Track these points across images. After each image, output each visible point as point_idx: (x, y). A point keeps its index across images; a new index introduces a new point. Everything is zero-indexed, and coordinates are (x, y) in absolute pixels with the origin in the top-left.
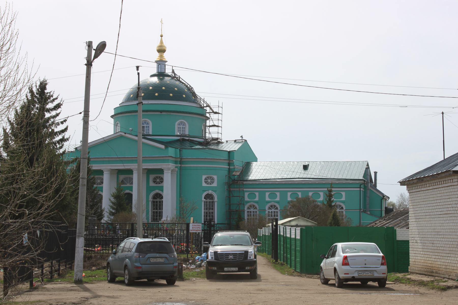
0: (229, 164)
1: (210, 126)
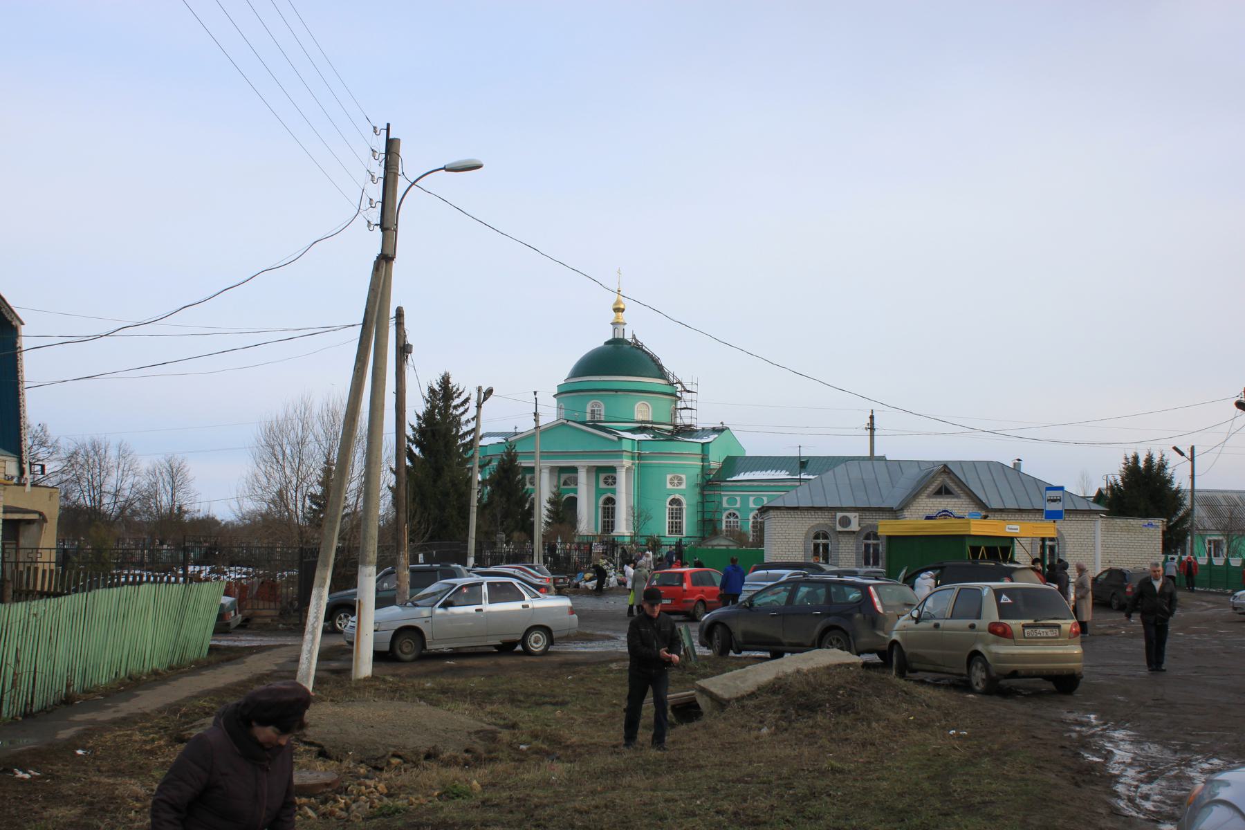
0: (703, 460)
1: (681, 409)
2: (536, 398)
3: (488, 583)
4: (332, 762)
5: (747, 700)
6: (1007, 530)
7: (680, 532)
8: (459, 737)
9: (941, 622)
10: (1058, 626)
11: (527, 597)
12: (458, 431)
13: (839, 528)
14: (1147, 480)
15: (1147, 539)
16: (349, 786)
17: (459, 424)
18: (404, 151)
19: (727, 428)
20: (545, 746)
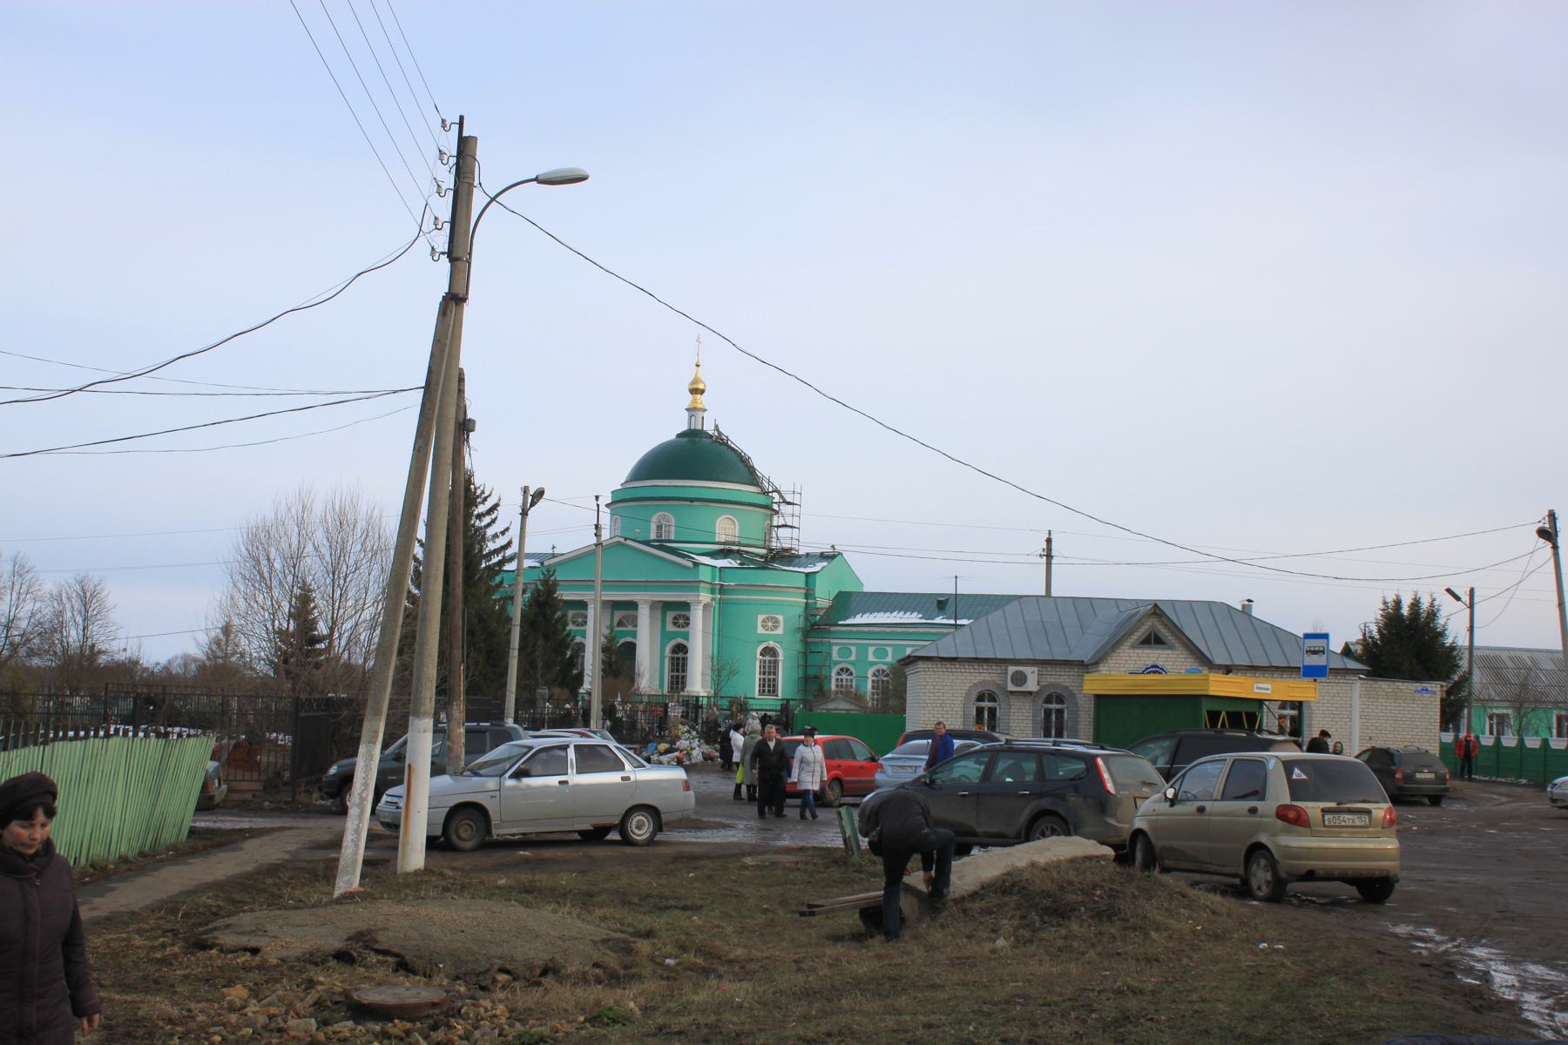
0: (807, 596)
1: (778, 527)
2: (598, 505)
3: (575, 746)
4: (417, 978)
5: (968, 901)
6: (1256, 690)
7: (774, 691)
8: (582, 947)
9: (1208, 805)
10: (1369, 812)
11: (628, 766)
12: (481, 550)
13: (1011, 687)
14: (1412, 632)
15: (1420, 709)
16: (462, 1007)
17: (484, 538)
18: (482, 153)
19: (839, 553)
20: (700, 961)
